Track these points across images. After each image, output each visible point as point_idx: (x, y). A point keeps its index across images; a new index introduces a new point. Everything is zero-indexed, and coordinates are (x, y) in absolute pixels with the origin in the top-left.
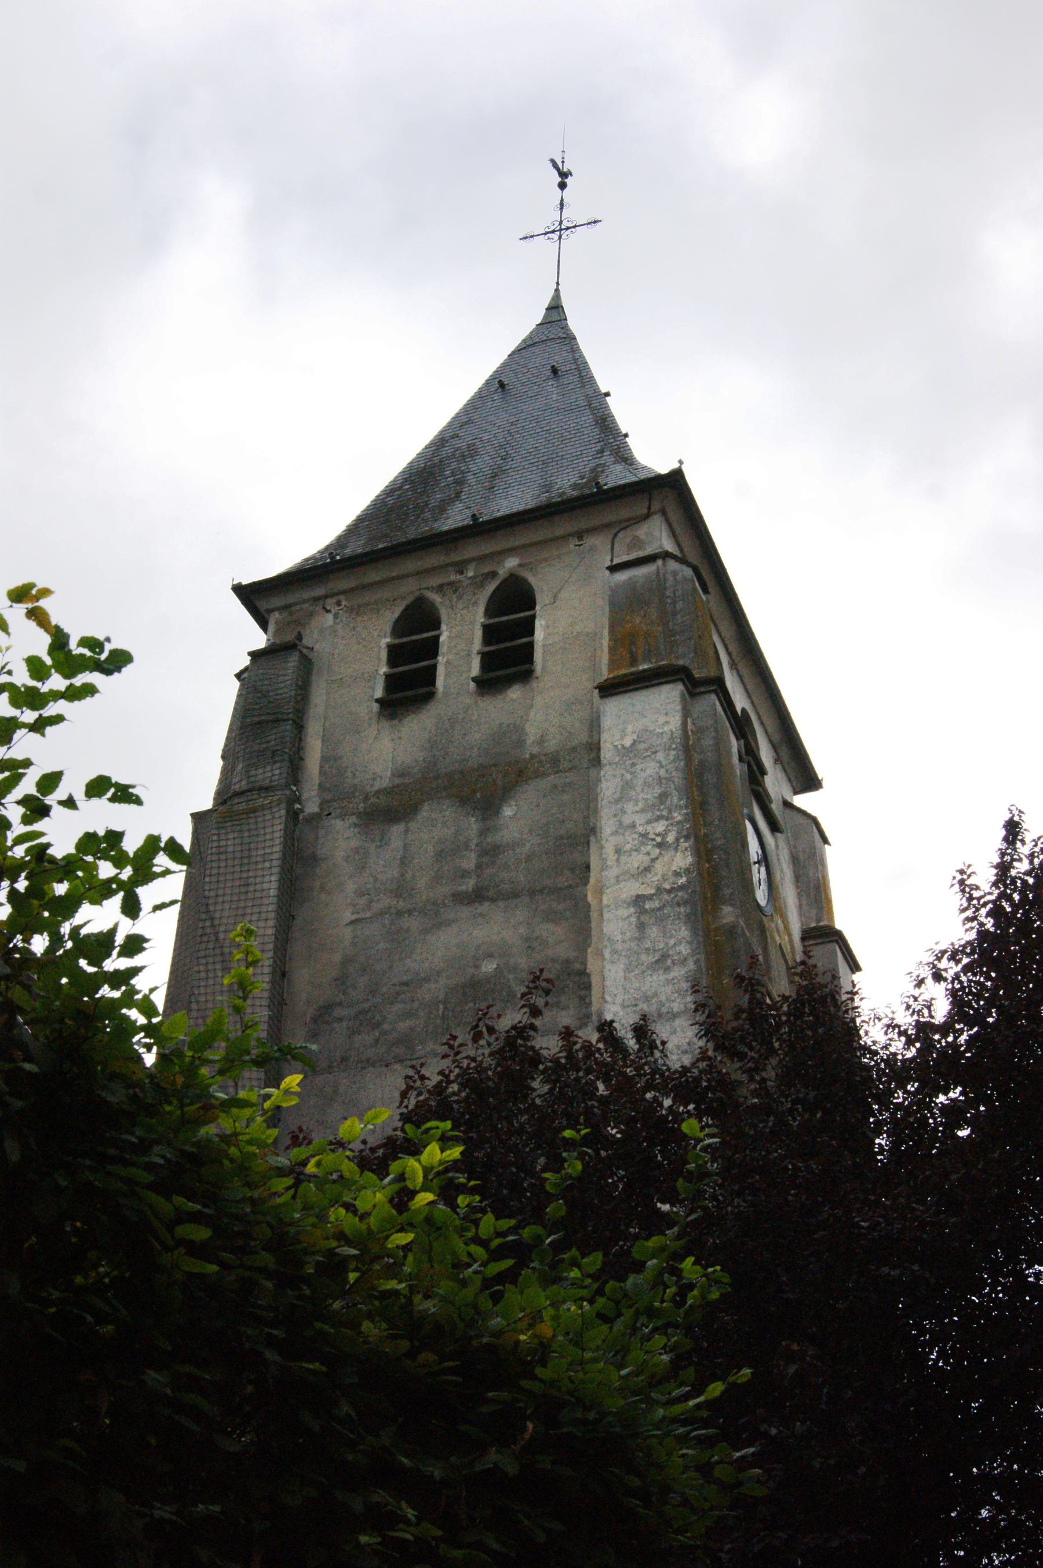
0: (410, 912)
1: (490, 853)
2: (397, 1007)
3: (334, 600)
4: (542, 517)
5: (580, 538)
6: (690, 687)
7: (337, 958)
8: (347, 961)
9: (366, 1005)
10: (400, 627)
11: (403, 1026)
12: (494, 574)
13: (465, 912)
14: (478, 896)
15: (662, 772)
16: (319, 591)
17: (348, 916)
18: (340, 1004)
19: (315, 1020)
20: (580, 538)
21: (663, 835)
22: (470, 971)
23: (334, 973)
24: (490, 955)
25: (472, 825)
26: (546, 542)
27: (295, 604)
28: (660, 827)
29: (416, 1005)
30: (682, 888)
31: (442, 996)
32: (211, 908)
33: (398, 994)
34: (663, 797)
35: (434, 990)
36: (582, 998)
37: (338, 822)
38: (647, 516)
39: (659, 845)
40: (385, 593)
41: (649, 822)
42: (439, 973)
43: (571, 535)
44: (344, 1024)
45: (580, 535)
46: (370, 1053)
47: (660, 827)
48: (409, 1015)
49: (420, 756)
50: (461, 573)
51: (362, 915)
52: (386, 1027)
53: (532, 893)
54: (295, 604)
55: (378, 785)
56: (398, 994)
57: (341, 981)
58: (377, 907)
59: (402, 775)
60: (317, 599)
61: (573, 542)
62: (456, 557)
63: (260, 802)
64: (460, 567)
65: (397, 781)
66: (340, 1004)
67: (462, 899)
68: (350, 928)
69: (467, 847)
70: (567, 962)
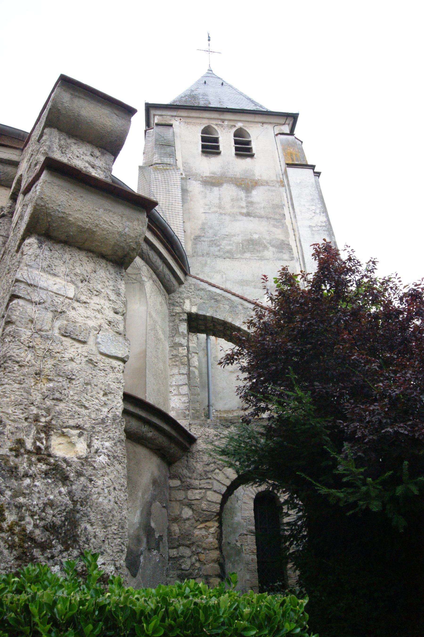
0: (225, 214)
1: (251, 203)
2: (225, 242)
3: (179, 118)
4: (253, 113)
5: (263, 124)
6: (285, 181)
7: (200, 222)
8: (204, 224)
9: (213, 239)
10: (204, 132)
11: (229, 248)
12: (235, 126)
13: (245, 218)
14: (248, 215)
15: (311, 193)
16: (174, 113)
17: (202, 210)
18: (203, 236)
19: (195, 239)
20: (263, 124)
21: (315, 210)
22: (249, 236)
23: (200, 227)
24: (256, 233)
25: (242, 194)
26: (251, 122)
27: (165, 115)
28: (314, 208)
29: (232, 242)
30: (324, 226)
31: (241, 242)
32: (155, 195)
33: (224, 238)
34: (313, 200)
35: (239, 239)
36: (290, 252)
37: (194, 182)
38: (284, 124)
39: (314, 213)
40: (198, 121)
41: (309, 205)
42: (238, 235)
43: (260, 122)
44: (206, 243)
45: (263, 123)
46: (217, 253)
47: (314, 208)
48: (229, 245)
49: (219, 170)
50: (223, 122)
51: (207, 211)
52: (222, 247)
53: (267, 218)
54: (165, 115)
55: (205, 175)
56: (224, 238)
57: (203, 229)
58: (212, 210)
59: (213, 174)
60: (172, 116)
61: (260, 125)
62: (222, 117)
63: (168, 168)
64: (223, 121)
65: (212, 175)
66: (203, 236)
67: (242, 214)
68: (204, 214)
69: (242, 199)
70: (283, 240)
